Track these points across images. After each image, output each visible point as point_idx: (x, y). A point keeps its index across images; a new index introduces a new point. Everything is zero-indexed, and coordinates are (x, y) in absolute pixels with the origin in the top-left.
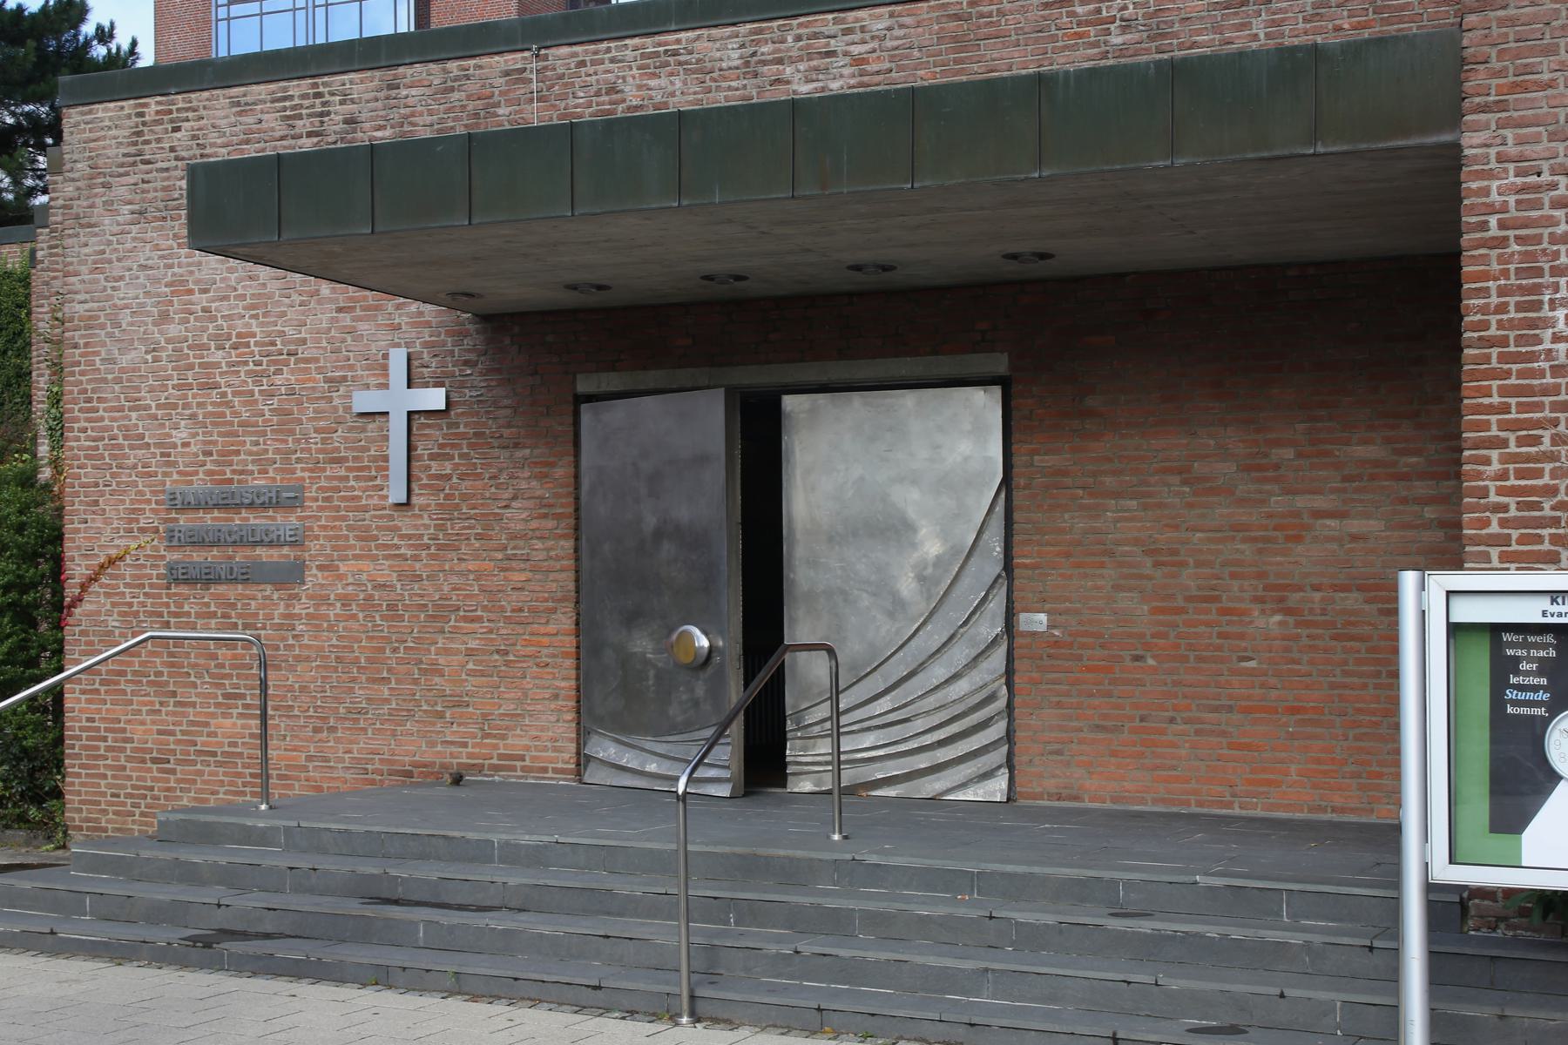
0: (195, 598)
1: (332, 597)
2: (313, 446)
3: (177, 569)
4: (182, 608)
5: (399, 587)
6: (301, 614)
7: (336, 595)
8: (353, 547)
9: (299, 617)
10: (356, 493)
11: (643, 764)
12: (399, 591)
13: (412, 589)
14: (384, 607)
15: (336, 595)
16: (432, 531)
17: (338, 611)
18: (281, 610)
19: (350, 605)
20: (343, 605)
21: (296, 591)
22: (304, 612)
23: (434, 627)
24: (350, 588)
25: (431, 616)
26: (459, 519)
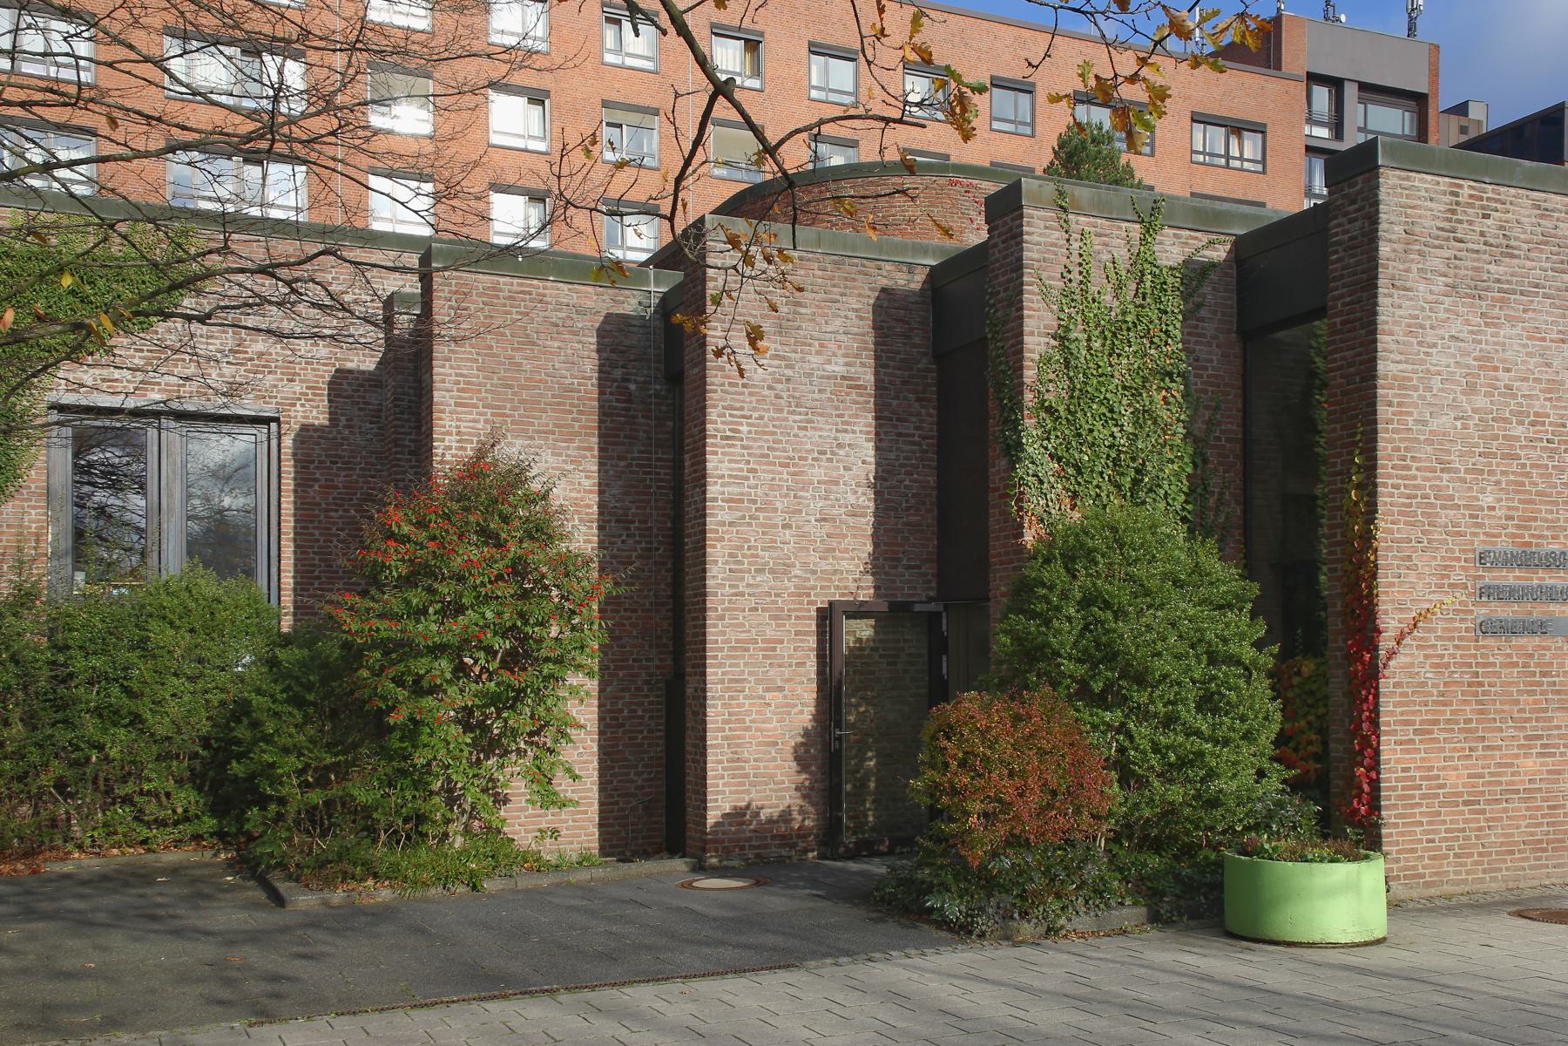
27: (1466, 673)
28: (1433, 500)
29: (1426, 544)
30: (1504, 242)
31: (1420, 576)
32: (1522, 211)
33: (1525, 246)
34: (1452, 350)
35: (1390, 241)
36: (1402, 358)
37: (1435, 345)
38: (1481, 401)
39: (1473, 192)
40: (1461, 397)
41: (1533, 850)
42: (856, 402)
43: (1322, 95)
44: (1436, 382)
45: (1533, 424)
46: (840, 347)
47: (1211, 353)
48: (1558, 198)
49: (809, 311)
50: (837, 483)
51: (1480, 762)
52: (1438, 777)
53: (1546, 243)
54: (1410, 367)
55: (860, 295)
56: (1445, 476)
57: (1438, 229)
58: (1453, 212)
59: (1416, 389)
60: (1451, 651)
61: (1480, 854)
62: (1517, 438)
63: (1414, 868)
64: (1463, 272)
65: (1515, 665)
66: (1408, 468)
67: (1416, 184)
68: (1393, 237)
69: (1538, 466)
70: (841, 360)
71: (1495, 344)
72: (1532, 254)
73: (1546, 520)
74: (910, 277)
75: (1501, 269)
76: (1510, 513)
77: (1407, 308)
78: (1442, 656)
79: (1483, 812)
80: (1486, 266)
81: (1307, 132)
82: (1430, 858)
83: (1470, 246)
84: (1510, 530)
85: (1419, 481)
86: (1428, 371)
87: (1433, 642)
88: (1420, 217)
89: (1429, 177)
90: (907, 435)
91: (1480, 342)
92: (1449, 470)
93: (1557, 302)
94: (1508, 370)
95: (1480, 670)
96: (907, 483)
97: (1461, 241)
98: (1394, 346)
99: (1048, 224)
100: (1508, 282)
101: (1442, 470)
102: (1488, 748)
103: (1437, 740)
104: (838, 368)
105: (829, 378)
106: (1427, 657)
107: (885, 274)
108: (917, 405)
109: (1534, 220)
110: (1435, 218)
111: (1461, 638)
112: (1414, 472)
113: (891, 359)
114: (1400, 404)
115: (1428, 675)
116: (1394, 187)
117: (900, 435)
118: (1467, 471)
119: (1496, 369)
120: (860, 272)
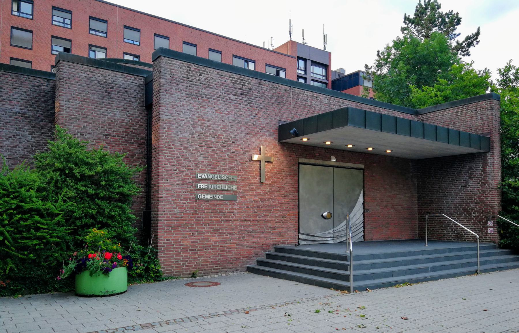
1: (244, 204)
8: (250, 192)
24: (249, 202)
27: (192, 211)
28: (180, 158)
29: (178, 171)
30: (207, 84)
31: (175, 181)
32: (214, 75)
33: (215, 85)
34: (188, 114)
35: (165, 79)
36: (169, 114)
37: (181, 112)
38: (199, 129)
39: (196, 68)
40: (191, 128)
41: (215, 264)
42: (24, 122)
43: (302, 63)
44: (182, 123)
45: (218, 138)
46: (18, 103)
47: (135, 112)
48: (226, 73)
49: (5, 91)
50: (16, 147)
51: (196, 238)
52: (180, 242)
53: (222, 85)
54: (172, 117)
55: (27, 87)
56: (185, 151)
57: (183, 77)
58: (188, 73)
59: (174, 124)
60: (187, 204)
61: (195, 265)
62: (212, 142)
63: (170, 270)
64: (192, 91)
65: (210, 209)
66: (171, 148)
67: (175, 63)
68: (166, 78)
69: (219, 150)
70: (19, 108)
71: (204, 113)
72: (217, 88)
73: (222, 166)
74: (48, 83)
75: (206, 91)
76: (209, 163)
77: (171, 100)
78: (183, 206)
79: (197, 253)
80: (201, 90)
81: (298, 72)
82: (176, 267)
83: (195, 83)
84: (209, 168)
85: (175, 152)
86: (179, 119)
87: (180, 201)
88: (176, 73)
89: (179, 61)
90: (46, 133)
91: (198, 112)
92: (186, 150)
93: (226, 103)
94: (209, 121)
95: (197, 210)
96: (45, 148)
97: (192, 82)
98: (166, 111)
99: (70, 67)
100: (209, 95)
101: (184, 149)
102: (200, 233)
103: (180, 231)
104: (17, 109)
105: (13, 113)
106: (177, 206)
107: (38, 81)
108: (50, 124)
109: (218, 78)
110: (181, 74)
111: (190, 200)
112: (173, 149)
113: (40, 109)
114: (168, 128)
115: (177, 211)
116: (166, 63)
117: (43, 133)
118: (193, 150)
119: (204, 120)
120: (27, 80)
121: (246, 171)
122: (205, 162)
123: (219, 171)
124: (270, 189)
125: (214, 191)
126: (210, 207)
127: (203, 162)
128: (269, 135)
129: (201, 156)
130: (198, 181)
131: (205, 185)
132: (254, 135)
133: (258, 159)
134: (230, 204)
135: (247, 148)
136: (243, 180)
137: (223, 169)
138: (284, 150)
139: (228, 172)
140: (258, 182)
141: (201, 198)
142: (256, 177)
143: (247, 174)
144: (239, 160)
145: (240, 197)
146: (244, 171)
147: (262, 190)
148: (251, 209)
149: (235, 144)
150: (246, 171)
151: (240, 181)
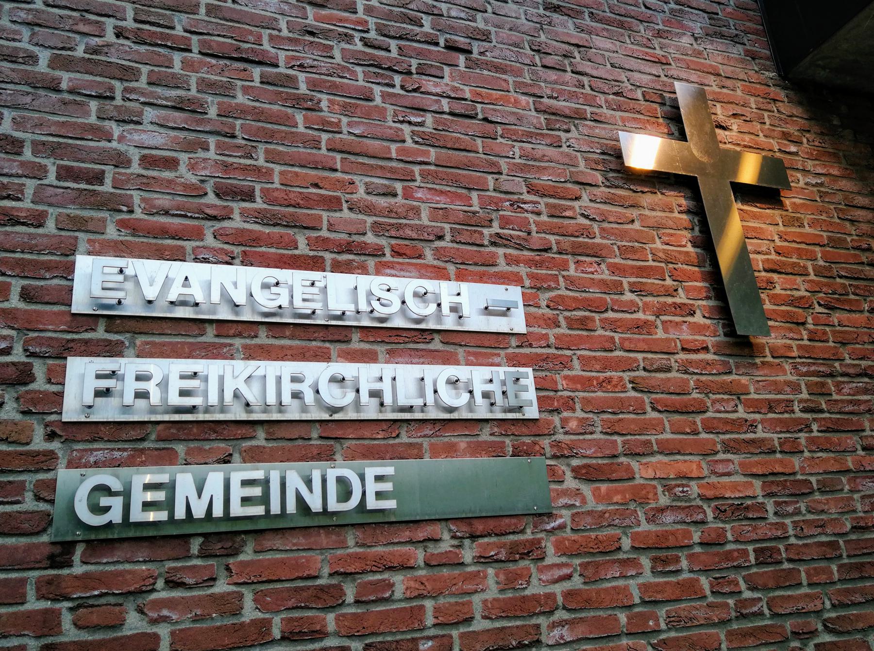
0: (172, 584)
1: (626, 543)
2: (532, 218)
3: (126, 494)
4: (118, 625)
5: (770, 508)
6: (551, 596)
7: (635, 537)
8: (656, 425)
9: (546, 603)
10: (640, 315)
11: (799, 490)
12: (773, 519)
13: (797, 512)
14: (752, 558)
15: (635, 537)
16: (805, 395)
17: (648, 577)
18: (492, 592)
19: (677, 560)
20: (654, 560)
21: (528, 535)
22: (558, 589)
23: (862, 591)
24: (669, 518)
25: (851, 567)
26: (844, 375)
84: (237, 223)
121: (597, 253)
122: (192, 167)
123: (348, 248)
124: (819, 391)
125: (295, 432)
126: (250, 613)
127: (171, 164)
128: (716, 32)
129: (150, 114)
130: (100, 333)
131: (371, 472)
132: (608, 21)
133: (659, 162)
134: (483, 560)
135: (572, 96)
136: (583, 324)
137: (378, 229)
138: (828, 132)
139: (429, 258)
140: (710, 341)
141: (115, 516)
142: (681, 298)
143: (606, 276)
144: (522, 168)
145: (577, 473)
146: (578, 251)
147: (755, 406)
148: (705, 582)
149: (472, 64)
150: (597, 253)
151: (552, 333)
